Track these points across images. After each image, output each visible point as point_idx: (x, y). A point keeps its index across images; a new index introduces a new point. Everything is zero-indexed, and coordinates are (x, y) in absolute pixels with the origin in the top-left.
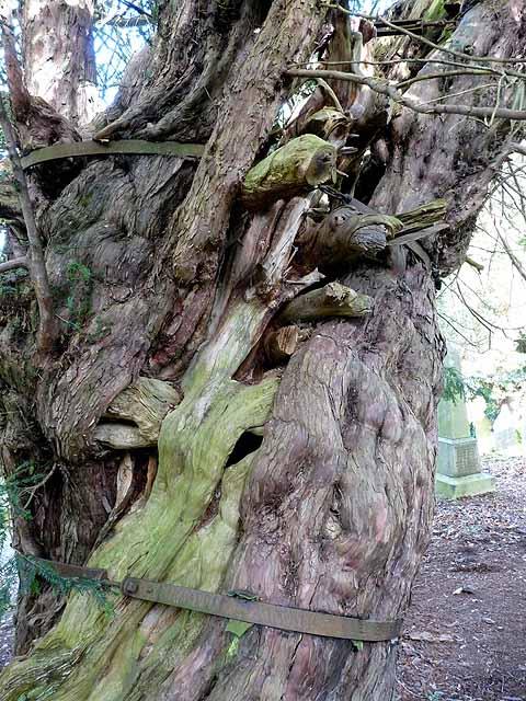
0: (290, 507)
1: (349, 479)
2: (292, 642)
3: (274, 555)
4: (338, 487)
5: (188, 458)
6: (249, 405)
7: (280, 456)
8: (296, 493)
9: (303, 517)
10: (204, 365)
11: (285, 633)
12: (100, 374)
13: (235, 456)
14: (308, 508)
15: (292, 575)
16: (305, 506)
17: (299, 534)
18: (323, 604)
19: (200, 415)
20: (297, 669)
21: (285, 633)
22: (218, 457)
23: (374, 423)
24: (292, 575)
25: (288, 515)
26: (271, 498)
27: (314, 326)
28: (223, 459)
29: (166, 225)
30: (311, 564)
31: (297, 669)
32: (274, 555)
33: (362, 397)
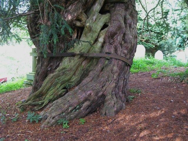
0: (116, 37)
1: (126, 32)
2: (118, 61)
3: (113, 47)
4: (124, 34)
5: (92, 29)
6: (104, 18)
7: (115, 27)
8: (117, 35)
9: (118, 39)
10: (93, 10)
11: (116, 59)
12: (77, 8)
13: (102, 29)
14: (119, 38)
15: (116, 50)
16: (119, 37)
17: (117, 43)
18: (122, 55)
19: (95, 20)
20: (119, 65)
21: (116, 59)
22: (99, 27)
23: (129, 24)
24: (116, 50)
25: (115, 39)
26: (112, 36)
27: (114, 4)
28: (100, 29)
29: (44, 106)
30: (120, 50)
31: (119, 65)
32: (113, 47)
33: (127, 18)
